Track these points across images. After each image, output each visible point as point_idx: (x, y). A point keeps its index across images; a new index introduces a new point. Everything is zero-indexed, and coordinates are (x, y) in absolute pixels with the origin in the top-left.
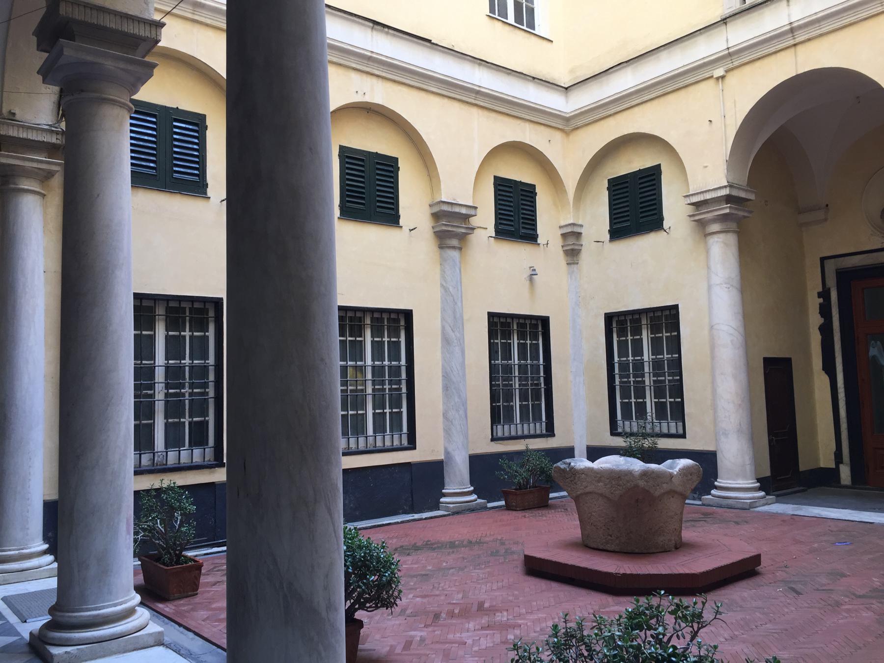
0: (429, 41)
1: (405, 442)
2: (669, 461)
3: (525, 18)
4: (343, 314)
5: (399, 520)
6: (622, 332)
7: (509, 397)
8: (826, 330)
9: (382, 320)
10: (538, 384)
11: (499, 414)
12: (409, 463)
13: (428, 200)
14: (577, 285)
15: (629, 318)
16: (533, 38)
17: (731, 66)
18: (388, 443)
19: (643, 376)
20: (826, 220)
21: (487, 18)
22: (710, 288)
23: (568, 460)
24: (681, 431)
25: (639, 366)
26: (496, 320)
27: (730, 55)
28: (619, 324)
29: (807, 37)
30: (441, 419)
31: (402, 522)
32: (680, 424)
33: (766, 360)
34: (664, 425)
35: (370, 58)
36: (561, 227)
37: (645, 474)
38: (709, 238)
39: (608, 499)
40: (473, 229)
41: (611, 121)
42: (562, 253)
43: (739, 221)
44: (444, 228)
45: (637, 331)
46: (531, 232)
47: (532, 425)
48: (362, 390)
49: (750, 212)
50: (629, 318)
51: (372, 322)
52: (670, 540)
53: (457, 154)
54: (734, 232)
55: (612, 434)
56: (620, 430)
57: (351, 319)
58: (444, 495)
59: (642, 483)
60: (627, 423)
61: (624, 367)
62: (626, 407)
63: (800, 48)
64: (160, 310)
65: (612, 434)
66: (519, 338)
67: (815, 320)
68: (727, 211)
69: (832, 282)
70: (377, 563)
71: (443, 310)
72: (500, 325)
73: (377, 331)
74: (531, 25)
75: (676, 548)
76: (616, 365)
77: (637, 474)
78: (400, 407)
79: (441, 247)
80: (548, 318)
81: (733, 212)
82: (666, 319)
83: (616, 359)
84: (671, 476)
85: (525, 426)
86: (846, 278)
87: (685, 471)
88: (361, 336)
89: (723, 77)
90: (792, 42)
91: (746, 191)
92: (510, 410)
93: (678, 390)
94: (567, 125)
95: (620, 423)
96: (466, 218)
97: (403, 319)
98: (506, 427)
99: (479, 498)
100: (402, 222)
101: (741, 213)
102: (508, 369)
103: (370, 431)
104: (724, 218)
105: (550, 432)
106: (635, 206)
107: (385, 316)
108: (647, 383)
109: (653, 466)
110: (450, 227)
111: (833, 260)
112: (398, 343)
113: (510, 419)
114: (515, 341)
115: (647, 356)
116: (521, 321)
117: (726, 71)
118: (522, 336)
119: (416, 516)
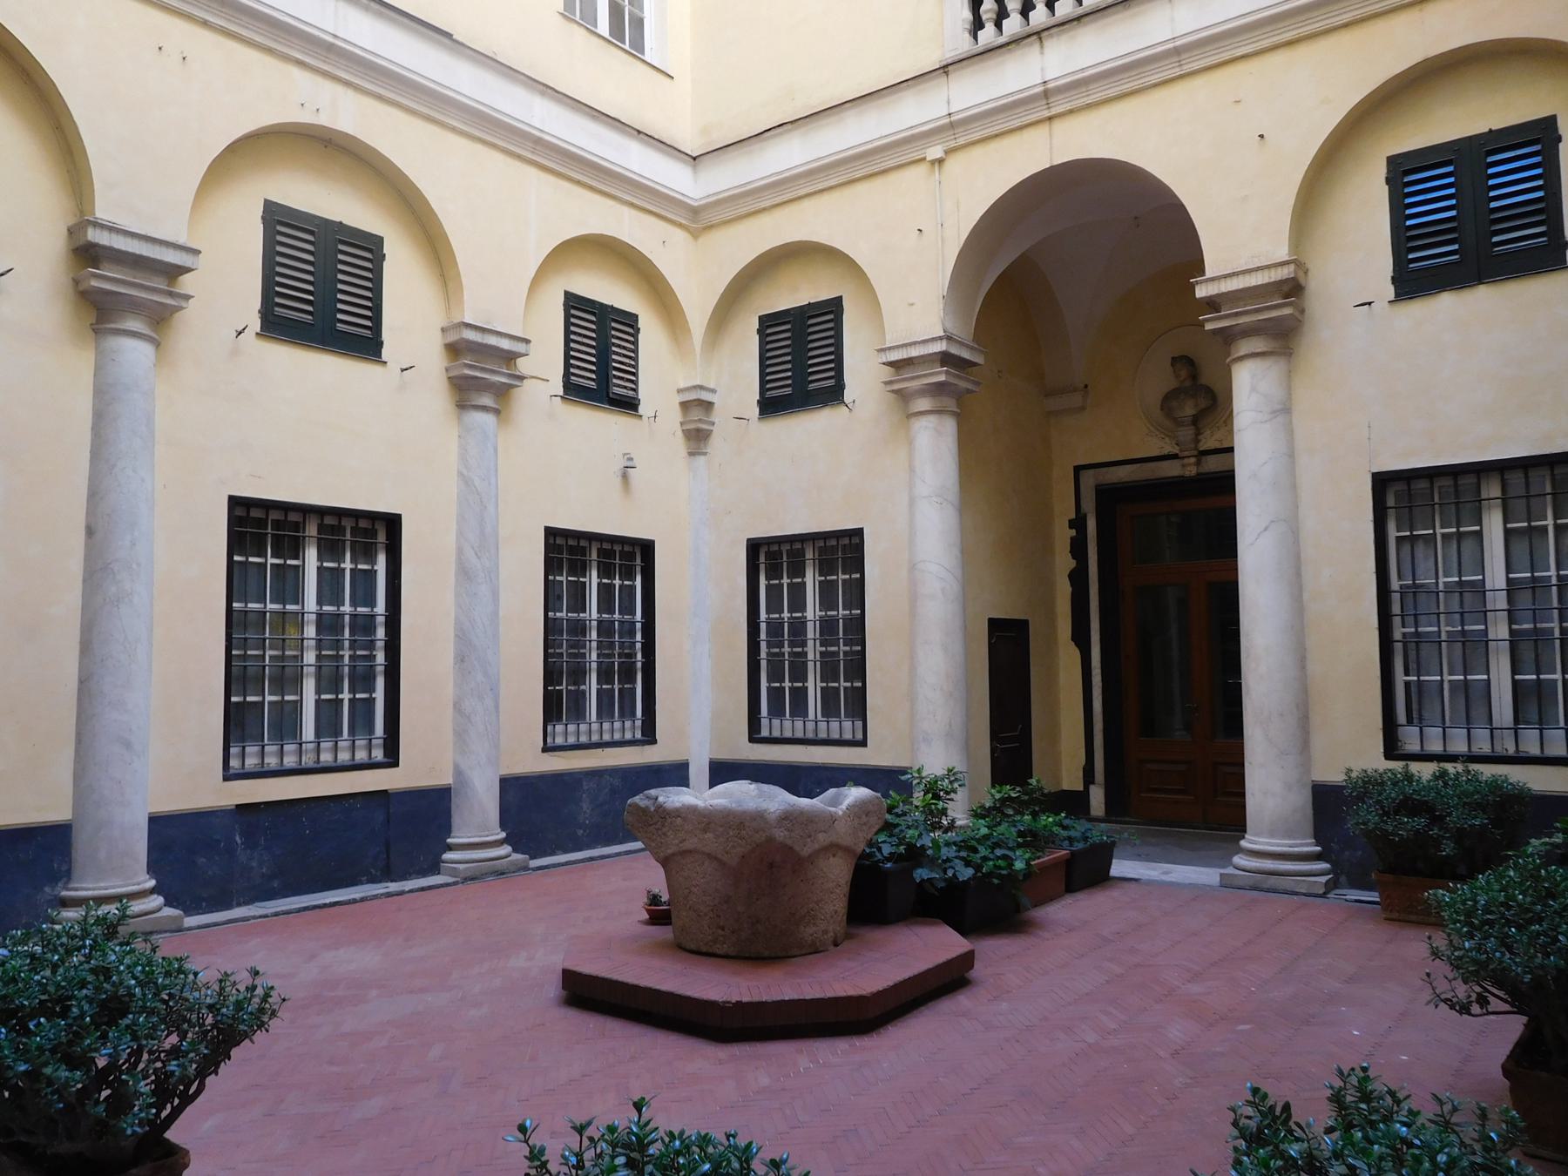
0: (448, 35)
1: (378, 754)
2: (832, 791)
3: (626, 30)
4: (240, 512)
5: (357, 896)
6: (774, 572)
7: (579, 674)
8: (1078, 578)
9: (341, 530)
10: (632, 655)
11: (558, 705)
12: (386, 791)
13: (439, 320)
14: (698, 490)
15: (785, 547)
16: (639, 63)
17: (953, 144)
18: (344, 757)
19: (804, 644)
20: (1083, 408)
21: (560, 18)
22: (912, 502)
23: (653, 792)
24: (859, 736)
25: (798, 628)
26: (559, 541)
27: (952, 125)
28: (770, 557)
29: (1067, 107)
30: (450, 710)
31: (363, 900)
32: (859, 724)
33: (990, 620)
34: (835, 725)
35: (330, 48)
36: (679, 391)
37: (788, 818)
38: (913, 420)
39: (722, 863)
40: (521, 378)
41: (765, 220)
42: (679, 433)
43: (960, 396)
44: (468, 372)
45: (798, 570)
46: (631, 393)
47: (617, 725)
48: (295, 657)
49: (977, 384)
50: (785, 547)
51: (319, 532)
52: (825, 932)
53: (500, 246)
54: (954, 414)
55: (752, 740)
56: (765, 733)
57: (277, 525)
58: (450, 848)
59: (780, 834)
60: (776, 722)
61: (775, 629)
62: (776, 696)
63: (1058, 126)
64: (312, 530)
65: (752, 740)
66: (597, 573)
67: (1064, 562)
68: (942, 378)
69: (1089, 506)
70: (186, 1032)
71: (461, 519)
72: (566, 550)
73: (330, 548)
74: (638, 44)
75: (836, 945)
76: (763, 626)
77: (773, 816)
78: (372, 689)
79: (462, 406)
80: (653, 542)
81: (952, 380)
82: (842, 551)
83: (763, 615)
84: (833, 819)
85: (606, 726)
86: (1110, 497)
87: (860, 809)
88: (297, 558)
89: (940, 161)
90: (1046, 114)
91: (972, 348)
92: (579, 699)
93: (857, 667)
94: (698, 219)
95: (764, 722)
96: (510, 358)
97: (379, 532)
98: (572, 728)
99: (515, 850)
100: (386, 353)
101: (963, 384)
102: (579, 628)
103: (309, 731)
104: (938, 389)
105: (649, 735)
106: (801, 362)
107: (348, 524)
108: (810, 656)
109: (804, 802)
110: (479, 372)
111: (1091, 472)
112: (372, 574)
113: (578, 713)
114: (593, 579)
115: (812, 611)
116: (606, 546)
117: (946, 152)
118: (606, 571)
119: (393, 887)
